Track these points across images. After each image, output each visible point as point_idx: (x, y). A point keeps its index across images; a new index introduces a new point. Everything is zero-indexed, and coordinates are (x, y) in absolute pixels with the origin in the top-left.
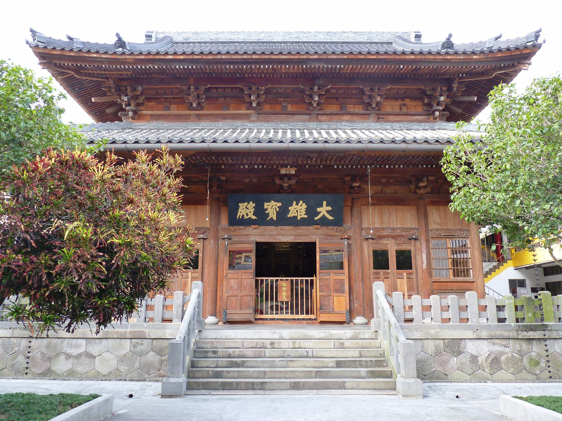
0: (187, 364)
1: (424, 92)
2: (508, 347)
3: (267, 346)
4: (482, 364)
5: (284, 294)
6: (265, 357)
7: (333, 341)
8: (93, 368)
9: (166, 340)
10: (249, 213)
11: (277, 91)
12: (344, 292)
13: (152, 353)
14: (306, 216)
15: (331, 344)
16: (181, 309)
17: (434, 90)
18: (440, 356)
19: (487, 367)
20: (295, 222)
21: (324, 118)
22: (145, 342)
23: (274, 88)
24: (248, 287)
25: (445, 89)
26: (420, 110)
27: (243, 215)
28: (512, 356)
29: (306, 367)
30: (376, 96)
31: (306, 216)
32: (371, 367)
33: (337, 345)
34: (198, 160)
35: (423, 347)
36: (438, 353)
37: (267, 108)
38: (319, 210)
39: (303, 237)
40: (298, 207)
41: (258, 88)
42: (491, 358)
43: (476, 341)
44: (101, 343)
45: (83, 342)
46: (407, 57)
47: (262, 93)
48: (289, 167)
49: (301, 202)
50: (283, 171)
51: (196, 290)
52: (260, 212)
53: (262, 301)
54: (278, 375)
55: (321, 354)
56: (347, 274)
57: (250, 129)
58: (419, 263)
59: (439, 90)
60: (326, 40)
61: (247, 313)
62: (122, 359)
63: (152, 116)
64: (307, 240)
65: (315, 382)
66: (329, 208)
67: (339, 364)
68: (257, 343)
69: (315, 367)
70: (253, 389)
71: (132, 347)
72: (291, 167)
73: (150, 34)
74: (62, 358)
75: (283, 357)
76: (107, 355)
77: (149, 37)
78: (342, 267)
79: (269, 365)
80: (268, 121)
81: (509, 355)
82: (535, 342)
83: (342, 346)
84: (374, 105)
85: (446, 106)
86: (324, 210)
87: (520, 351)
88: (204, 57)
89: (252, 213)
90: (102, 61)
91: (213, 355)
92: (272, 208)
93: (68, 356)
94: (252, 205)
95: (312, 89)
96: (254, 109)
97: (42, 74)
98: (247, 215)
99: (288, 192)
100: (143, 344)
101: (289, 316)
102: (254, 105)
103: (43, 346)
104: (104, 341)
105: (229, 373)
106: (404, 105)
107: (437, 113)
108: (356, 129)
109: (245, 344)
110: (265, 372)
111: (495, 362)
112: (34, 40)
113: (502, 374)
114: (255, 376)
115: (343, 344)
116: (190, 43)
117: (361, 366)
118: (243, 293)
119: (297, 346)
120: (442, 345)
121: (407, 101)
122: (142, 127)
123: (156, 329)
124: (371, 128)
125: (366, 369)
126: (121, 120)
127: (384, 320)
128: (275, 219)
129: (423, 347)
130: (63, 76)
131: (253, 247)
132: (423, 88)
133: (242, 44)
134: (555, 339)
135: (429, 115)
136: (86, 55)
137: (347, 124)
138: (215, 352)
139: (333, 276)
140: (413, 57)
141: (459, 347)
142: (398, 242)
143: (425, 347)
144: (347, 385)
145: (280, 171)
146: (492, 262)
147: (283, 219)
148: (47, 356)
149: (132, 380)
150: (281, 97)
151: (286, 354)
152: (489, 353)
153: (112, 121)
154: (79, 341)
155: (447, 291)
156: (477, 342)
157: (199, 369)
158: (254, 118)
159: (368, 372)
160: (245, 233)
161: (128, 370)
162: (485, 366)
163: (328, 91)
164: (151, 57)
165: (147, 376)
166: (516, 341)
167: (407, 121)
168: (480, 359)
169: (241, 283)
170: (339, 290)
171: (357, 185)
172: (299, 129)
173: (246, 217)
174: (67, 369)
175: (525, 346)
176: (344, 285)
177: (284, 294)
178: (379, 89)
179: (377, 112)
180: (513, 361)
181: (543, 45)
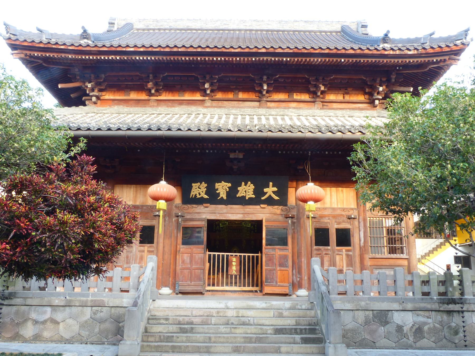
0: (141, 330)
1: (365, 83)
2: (430, 318)
3: (214, 315)
4: (406, 333)
5: (234, 268)
7: (272, 311)
8: (57, 332)
9: (123, 308)
10: (201, 193)
11: (230, 79)
14: (254, 196)
15: (271, 313)
16: (137, 281)
17: (374, 80)
18: (369, 326)
19: (411, 336)
20: (243, 201)
21: (273, 104)
23: (227, 77)
24: (199, 261)
25: (384, 79)
27: (196, 194)
28: (434, 326)
29: (247, 334)
30: (321, 86)
31: (254, 196)
33: (276, 314)
34: (155, 145)
35: (354, 317)
36: (367, 322)
37: (219, 95)
38: (265, 190)
39: (251, 216)
40: (247, 188)
41: (212, 77)
42: (415, 328)
43: (402, 312)
44: (64, 310)
45: (49, 309)
47: (216, 81)
48: (237, 152)
50: (232, 156)
51: (152, 263)
52: (212, 192)
53: (214, 274)
56: (290, 250)
57: (204, 114)
59: (378, 81)
62: (82, 326)
64: (254, 218)
65: (254, 347)
66: (275, 189)
69: (255, 334)
71: (92, 314)
72: (239, 152)
73: (113, 22)
74: (30, 324)
76: (70, 321)
77: (112, 24)
78: (285, 244)
79: (214, 331)
81: (432, 326)
82: (455, 314)
83: (281, 316)
86: (270, 190)
87: (441, 322)
88: (162, 50)
89: (204, 192)
91: (165, 322)
92: (222, 188)
93: (36, 322)
94: (204, 185)
95: (262, 78)
98: (200, 194)
99: (236, 175)
100: (102, 312)
102: (208, 92)
103: (12, 313)
104: (67, 308)
105: (178, 338)
107: (377, 102)
108: (302, 116)
111: (418, 331)
112: (7, 33)
113: (424, 342)
114: (201, 341)
116: (151, 29)
117: (297, 333)
119: (240, 315)
120: (371, 316)
122: (104, 111)
124: (315, 115)
125: (300, 336)
126: (85, 105)
127: (319, 292)
128: (225, 198)
130: (32, 64)
131: (204, 224)
132: (365, 78)
133: (199, 32)
134: (473, 311)
136: (54, 46)
137: (294, 110)
138: (167, 319)
141: (386, 317)
143: (356, 317)
145: (229, 155)
146: (439, 238)
147: (233, 199)
148: (16, 322)
149: (93, 344)
150: (233, 85)
151: (230, 322)
152: (413, 323)
153: (77, 105)
155: (381, 267)
156: (403, 314)
157: (151, 334)
159: (302, 338)
160: (198, 211)
161: (89, 335)
162: (409, 335)
163: (276, 80)
164: (113, 49)
165: (106, 340)
166: (437, 313)
167: (349, 109)
168: (405, 329)
171: (301, 168)
172: (249, 115)
173: (198, 196)
175: (445, 317)
176: (287, 260)
177: (234, 268)
178: (323, 79)
179: (322, 100)
180: (433, 331)
181: (471, 43)
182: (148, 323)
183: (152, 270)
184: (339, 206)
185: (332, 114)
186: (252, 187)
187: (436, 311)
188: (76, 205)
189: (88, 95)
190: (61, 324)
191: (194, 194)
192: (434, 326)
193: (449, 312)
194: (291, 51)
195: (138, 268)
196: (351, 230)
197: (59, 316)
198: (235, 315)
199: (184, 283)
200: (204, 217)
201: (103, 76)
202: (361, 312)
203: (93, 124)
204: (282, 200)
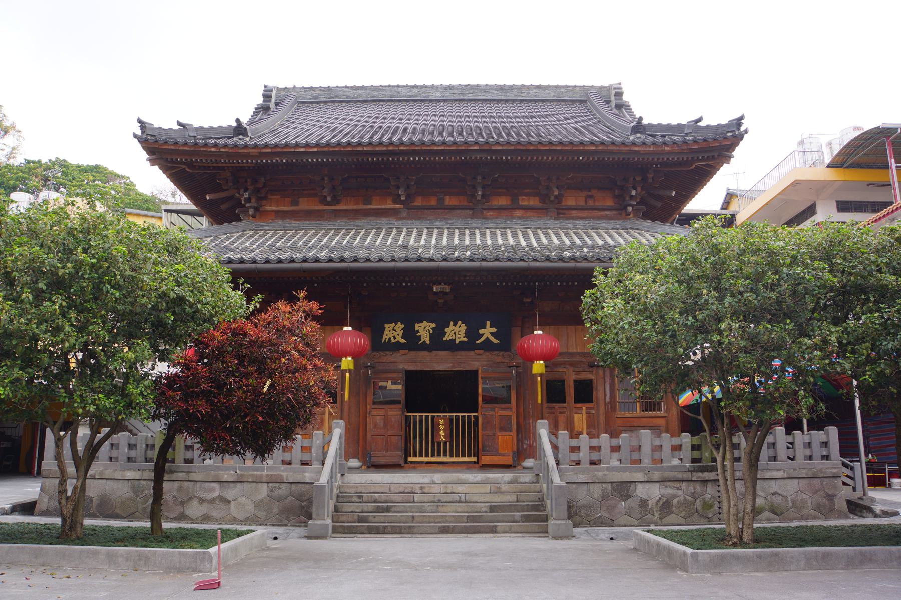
5: (442, 433)
6: (414, 502)
12: (511, 431)
13: (290, 498)
14: (466, 340)
15: (487, 488)
21: (491, 213)
22: (283, 486)
25: (638, 179)
26: (609, 203)
28: (685, 499)
31: (466, 340)
32: (527, 511)
35: (588, 491)
36: (604, 497)
38: (481, 332)
40: (457, 329)
42: (661, 502)
43: (647, 484)
44: (235, 487)
46: (586, 148)
49: (460, 322)
52: (410, 334)
54: (427, 520)
55: (475, 499)
56: (514, 410)
57: (397, 229)
58: (601, 395)
60: (500, 98)
61: (396, 456)
62: (258, 505)
63: (277, 212)
66: (494, 330)
67: (492, 509)
68: (406, 488)
70: (401, 533)
74: (195, 502)
75: (434, 502)
76: (242, 500)
80: (419, 219)
81: (682, 498)
83: (499, 492)
84: (552, 198)
85: (641, 199)
86: (487, 332)
87: (693, 494)
90: (221, 155)
91: (358, 500)
92: (424, 330)
93: (202, 501)
94: (400, 326)
95: (474, 178)
96: (402, 202)
97: (154, 182)
98: (395, 338)
101: (448, 459)
104: (239, 485)
106: (591, 197)
107: (630, 209)
109: (392, 489)
110: (413, 517)
111: (666, 507)
112: (143, 133)
115: (499, 488)
118: (390, 433)
119: (449, 491)
121: (594, 193)
123: (295, 472)
126: (239, 220)
128: (428, 342)
129: (588, 491)
135: (622, 210)
137: (519, 221)
139: (499, 412)
140: (593, 148)
141: (628, 491)
142: (576, 370)
144: (498, 529)
147: (438, 343)
153: (230, 222)
154: (213, 485)
156: (648, 486)
158: (404, 214)
159: (521, 516)
160: (393, 360)
164: (279, 150)
167: (593, 218)
168: (650, 503)
169: (386, 420)
170: (505, 428)
173: (393, 341)
174: (202, 514)
175: (699, 488)
177: (442, 433)
178: (558, 179)
180: (685, 504)
182: (337, 502)
183: (340, 438)
184: (579, 351)
185: (570, 226)
186: (464, 327)
187: (688, 481)
188: (173, 328)
189: (244, 206)
190: (233, 503)
191: (388, 338)
192: (685, 499)
193: (704, 482)
194: (512, 148)
195: (321, 436)
196: (594, 382)
197: (230, 494)
198: (443, 491)
199: (380, 454)
200: (401, 367)
201: (263, 180)
202: (597, 486)
203: (257, 255)
204: (505, 344)
